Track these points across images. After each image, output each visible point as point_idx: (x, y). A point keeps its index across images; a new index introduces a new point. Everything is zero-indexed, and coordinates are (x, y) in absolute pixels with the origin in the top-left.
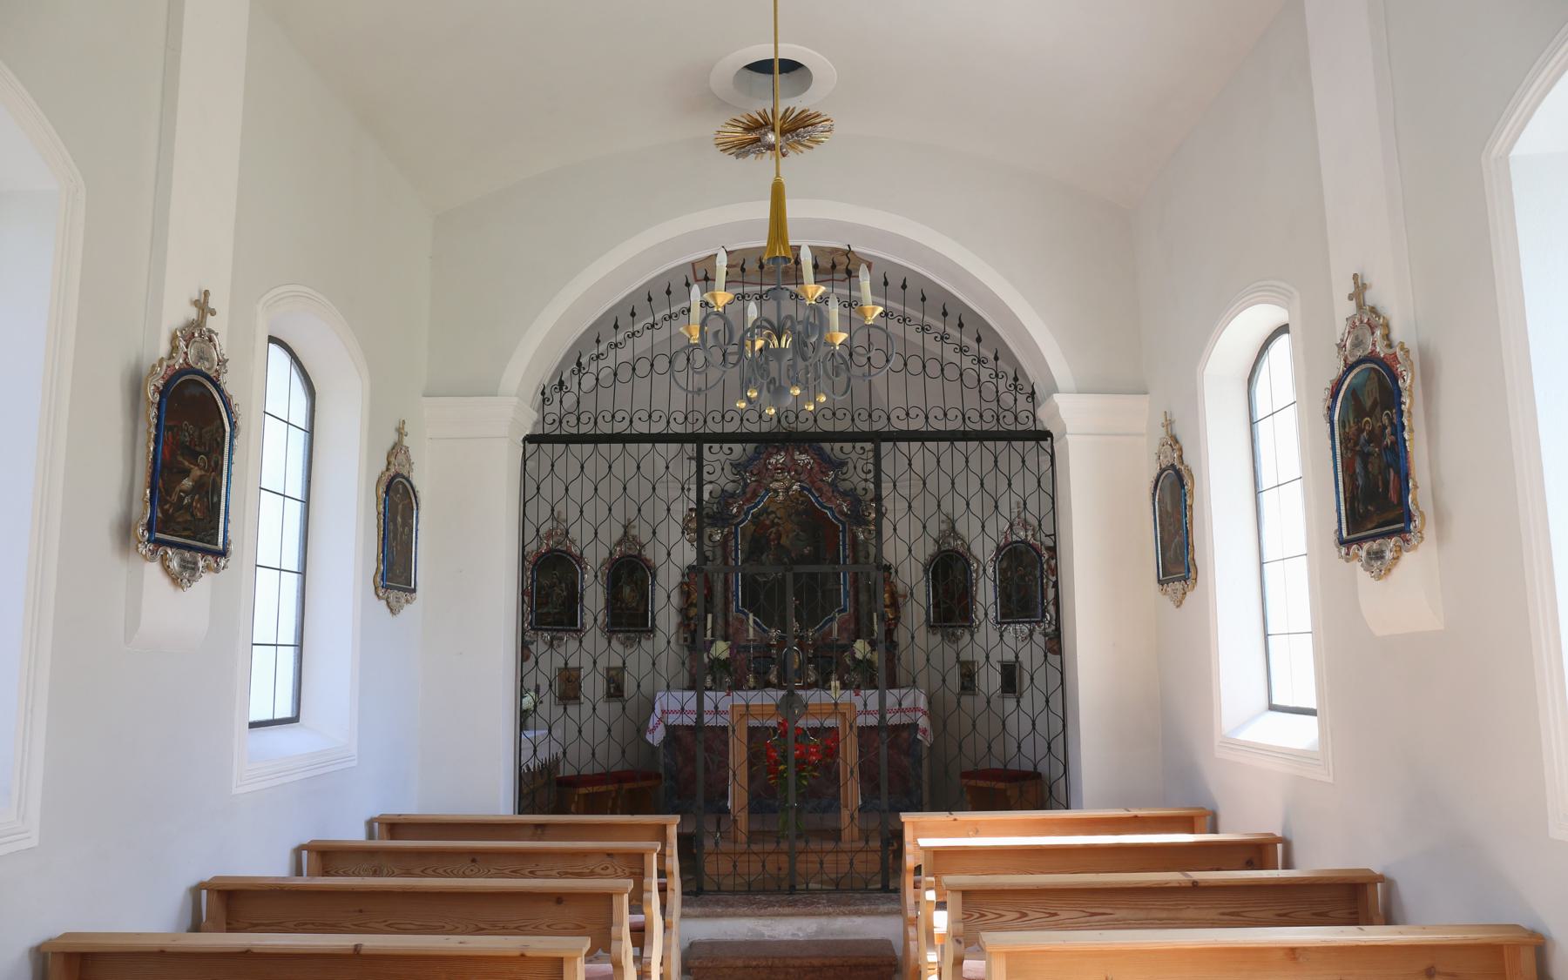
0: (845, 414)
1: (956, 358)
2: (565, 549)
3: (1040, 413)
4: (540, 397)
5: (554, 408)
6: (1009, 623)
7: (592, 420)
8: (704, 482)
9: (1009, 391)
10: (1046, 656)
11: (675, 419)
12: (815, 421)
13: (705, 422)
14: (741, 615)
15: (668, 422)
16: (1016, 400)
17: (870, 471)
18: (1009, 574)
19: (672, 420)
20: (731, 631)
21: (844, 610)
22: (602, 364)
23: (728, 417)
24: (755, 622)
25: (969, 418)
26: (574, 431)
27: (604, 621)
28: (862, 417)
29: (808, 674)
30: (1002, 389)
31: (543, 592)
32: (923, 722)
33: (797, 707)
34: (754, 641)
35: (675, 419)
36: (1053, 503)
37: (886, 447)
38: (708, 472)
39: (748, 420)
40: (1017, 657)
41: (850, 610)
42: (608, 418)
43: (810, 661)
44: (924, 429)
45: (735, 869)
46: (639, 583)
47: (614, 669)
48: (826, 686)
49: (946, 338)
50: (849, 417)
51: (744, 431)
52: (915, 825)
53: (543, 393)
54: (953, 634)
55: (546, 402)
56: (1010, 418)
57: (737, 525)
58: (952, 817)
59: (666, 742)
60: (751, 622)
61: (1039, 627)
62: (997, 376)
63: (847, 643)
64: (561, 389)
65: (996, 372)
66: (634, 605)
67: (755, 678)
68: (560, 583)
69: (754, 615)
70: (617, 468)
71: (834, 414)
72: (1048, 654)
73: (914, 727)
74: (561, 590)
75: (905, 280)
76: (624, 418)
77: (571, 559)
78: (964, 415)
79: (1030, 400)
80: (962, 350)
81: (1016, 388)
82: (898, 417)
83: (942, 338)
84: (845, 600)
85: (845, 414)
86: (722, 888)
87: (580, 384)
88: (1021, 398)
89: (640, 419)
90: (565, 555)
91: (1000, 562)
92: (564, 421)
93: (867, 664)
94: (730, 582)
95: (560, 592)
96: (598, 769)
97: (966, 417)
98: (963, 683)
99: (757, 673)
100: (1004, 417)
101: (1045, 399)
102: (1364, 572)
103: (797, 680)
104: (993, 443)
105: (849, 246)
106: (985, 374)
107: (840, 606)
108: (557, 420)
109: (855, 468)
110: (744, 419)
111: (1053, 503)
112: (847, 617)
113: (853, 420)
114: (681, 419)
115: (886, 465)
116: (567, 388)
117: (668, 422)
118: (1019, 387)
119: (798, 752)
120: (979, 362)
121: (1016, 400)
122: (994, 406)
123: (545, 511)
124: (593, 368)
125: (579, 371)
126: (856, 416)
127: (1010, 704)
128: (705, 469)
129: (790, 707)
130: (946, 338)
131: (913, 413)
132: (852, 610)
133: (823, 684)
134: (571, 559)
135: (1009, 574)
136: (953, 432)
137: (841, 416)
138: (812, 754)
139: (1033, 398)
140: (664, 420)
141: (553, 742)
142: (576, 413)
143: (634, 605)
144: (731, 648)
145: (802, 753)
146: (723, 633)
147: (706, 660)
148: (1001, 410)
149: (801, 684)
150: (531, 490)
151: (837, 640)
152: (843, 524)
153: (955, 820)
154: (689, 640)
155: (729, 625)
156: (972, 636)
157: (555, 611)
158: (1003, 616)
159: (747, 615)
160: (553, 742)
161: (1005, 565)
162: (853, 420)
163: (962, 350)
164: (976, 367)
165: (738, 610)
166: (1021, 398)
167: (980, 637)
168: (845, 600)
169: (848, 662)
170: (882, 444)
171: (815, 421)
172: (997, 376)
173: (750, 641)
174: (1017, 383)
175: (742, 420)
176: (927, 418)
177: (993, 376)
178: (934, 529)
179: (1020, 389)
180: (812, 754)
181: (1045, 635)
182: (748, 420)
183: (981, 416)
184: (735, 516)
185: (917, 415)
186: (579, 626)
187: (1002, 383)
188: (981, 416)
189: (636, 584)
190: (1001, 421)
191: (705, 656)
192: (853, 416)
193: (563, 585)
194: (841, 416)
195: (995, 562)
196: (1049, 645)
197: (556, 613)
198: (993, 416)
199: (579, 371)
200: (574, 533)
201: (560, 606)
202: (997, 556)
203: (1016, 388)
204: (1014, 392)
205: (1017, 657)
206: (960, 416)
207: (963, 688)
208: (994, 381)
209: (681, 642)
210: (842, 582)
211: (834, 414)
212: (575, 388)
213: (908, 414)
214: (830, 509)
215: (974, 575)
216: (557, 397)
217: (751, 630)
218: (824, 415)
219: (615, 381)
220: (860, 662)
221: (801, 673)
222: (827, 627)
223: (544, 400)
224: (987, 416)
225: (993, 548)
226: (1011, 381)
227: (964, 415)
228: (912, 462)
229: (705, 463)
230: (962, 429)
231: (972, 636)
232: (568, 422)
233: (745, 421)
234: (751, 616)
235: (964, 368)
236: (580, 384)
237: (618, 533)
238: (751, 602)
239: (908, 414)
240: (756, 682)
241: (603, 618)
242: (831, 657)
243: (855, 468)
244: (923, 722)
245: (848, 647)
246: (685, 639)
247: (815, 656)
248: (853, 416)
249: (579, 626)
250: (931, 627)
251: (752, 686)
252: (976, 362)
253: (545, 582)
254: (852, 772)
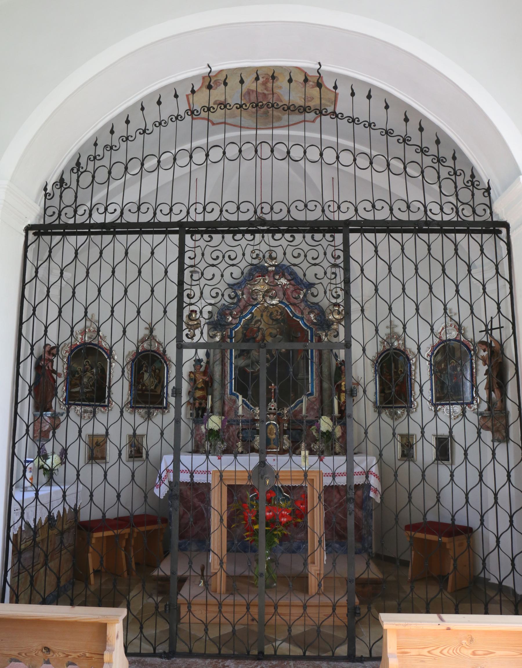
0: (316, 206)
1: (417, 157)
2: (96, 342)
3: (496, 207)
4: (44, 192)
5: (56, 201)
6: (443, 405)
7: (88, 212)
8: (186, 266)
9: (467, 187)
10: (479, 433)
11: (161, 211)
12: (289, 211)
13: (188, 213)
14: (234, 397)
15: (155, 214)
16: (473, 195)
17: (339, 257)
18: (443, 365)
19: (158, 211)
20: (226, 408)
21: (311, 394)
22: (98, 163)
23: (209, 209)
24: (243, 401)
25: (430, 210)
26: (71, 221)
27: (128, 399)
28: (331, 209)
29: (283, 443)
30: (460, 184)
31: (77, 375)
32: (374, 481)
33: (268, 478)
34: (243, 416)
35: (161, 211)
36: (511, 288)
37: (353, 237)
38: (189, 258)
39: (227, 211)
40: (451, 432)
41: (316, 394)
42: (102, 210)
43: (285, 432)
44: (389, 219)
45: (206, 633)
46: (157, 371)
47: (98, 436)
48: (297, 452)
49: (408, 140)
50: (319, 208)
51: (223, 219)
52: (398, 632)
53: (45, 189)
54: (396, 413)
55: (48, 197)
56: (468, 211)
57: (232, 330)
58: (443, 626)
59: (170, 495)
60: (240, 402)
61: (470, 408)
62: (455, 173)
63: (314, 419)
64: (61, 186)
65: (454, 170)
66: (153, 387)
67: (243, 445)
68: (92, 368)
69: (243, 397)
70: (107, 254)
71: (306, 206)
72: (482, 430)
73: (367, 486)
74: (93, 374)
75: (370, 91)
76: (115, 210)
77: (101, 350)
78: (425, 207)
79: (486, 194)
80: (423, 151)
81: (473, 184)
82: (365, 209)
83: (404, 141)
84: (313, 386)
85: (316, 206)
86: (193, 651)
87: (78, 181)
88: (478, 194)
89: (130, 210)
90: (97, 348)
91: (435, 356)
92: (63, 213)
93: (328, 436)
94: (226, 373)
95: (91, 376)
96: (123, 513)
97: (428, 209)
98: (403, 452)
99: (244, 440)
100: (463, 209)
101: (499, 195)
102: (481, 407)
103: (275, 447)
104: (453, 235)
105: (319, 63)
106: (444, 172)
107: (308, 391)
108: (57, 212)
109: (325, 254)
110: (224, 209)
111: (511, 288)
112: (314, 399)
113: (323, 211)
114: (166, 210)
115: (354, 251)
116: (66, 185)
117: (155, 214)
118: (476, 183)
119: (271, 514)
120: (439, 161)
121: (473, 195)
122: (453, 199)
123: (79, 313)
124: (90, 168)
125: (78, 170)
126: (326, 208)
127: (444, 471)
128: (187, 255)
129: (262, 478)
130: (408, 140)
131: (378, 205)
132: (317, 395)
133: (295, 450)
134: (101, 350)
135: (443, 365)
136: (417, 223)
137: (313, 208)
138: (283, 516)
139: (489, 194)
140: (151, 212)
141: (39, 506)
142: (74, 206)
143: (153, 387)
144: (223, 422)
145: (274, 515)
146: (220, 410)
147: (204, 430)
148: (459, 204)
149: (278, 450)
150: (30, 273)
151: (307, 416)
152: (311, 329)
153: (449, 629)
154: (195, 415)
155: (225, 404)
156: (408, 415)
157: (88, 390)
158: (437, 399)
159: (238, 397)
160: (39, 506)
161: (439, 358)
162: (323, 211)
163: (423, 151)
164: (436, 166)
165: (231, 393)
166: (478, 194)
167: (416, 416)
168: (313, 386)
169: (314, 434)
170: (351, 235)
171: (289, 211)
172: (455, 173)
173: (239, 416)
174: (474, 180)
175: (221, 211)
176: (391, 209)
177: (452, 173)
178: (384, 331)
179: (477, 185)
180: (283, 516)
181: (479, 414)
182: (227, 211)
183: (442, 209)
184: (231, 323)
185: (383, 207)
186: (106, 403)
187: (460, 180)
188: (442, 209)
189: (155, 372)
190: (460, 213)
191: (203, 427)
192: (323, 208)
193: (94, 370)
194: (313, 208)
195: (431, 357)
196: (482, 422)
197: (87, 392)
198: (452, 209)
199: (78, 170)
200: (105, 331)
201: (91, 386)
202: (432, 351)
203: (473, 184)
204: (471, 188)
205: (451, 432)
206: (422, 208)
207: (403, 455)
208: (453, 177)
209: (189, 416)
210: (310, 382)
211: (306, 206)
212: (74, 185)
213: (374, 206)
214: (302, 319)
215: (413, 367)
216: (58, 192)
217: (240, 408)
218: (296, 207)
219: (109, 178)
220: (323, 433)
221: (279, 442)
222: (298, 407)
223: (46, 195)
224: (447, 209)
225: (429, 346)
226: (468, 178)
227: (425, 207)
228: (378, 249)
229: (187, 249)
230: (424, 219)
231: (408, 415)
232: (66, 214)
233: (224, 213)
234: (240, 397)
235: (410, 201)
236: (78, 181)
237: (143, 332)
238: (241, 389)
239: (374, 206)
240: (243, 448)
241: (127, 397)
242: (302, 430)
243: (325, 254)
244: (374, 481)
245: (315, 422)
246: (191, 415)
247: (288, 429)
248: (323, 208)
249: (106, 403)
250: (379, 408)
251: (337, 452)
252: (435, 161)
253: (79, 368)
254: (320, 542)
